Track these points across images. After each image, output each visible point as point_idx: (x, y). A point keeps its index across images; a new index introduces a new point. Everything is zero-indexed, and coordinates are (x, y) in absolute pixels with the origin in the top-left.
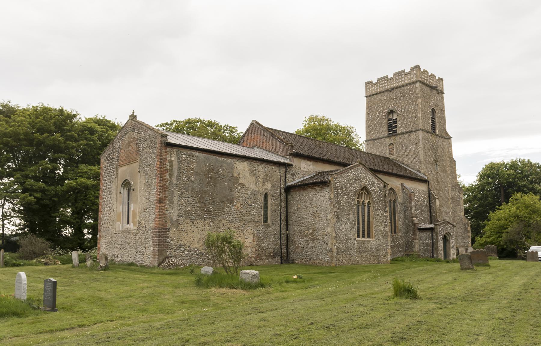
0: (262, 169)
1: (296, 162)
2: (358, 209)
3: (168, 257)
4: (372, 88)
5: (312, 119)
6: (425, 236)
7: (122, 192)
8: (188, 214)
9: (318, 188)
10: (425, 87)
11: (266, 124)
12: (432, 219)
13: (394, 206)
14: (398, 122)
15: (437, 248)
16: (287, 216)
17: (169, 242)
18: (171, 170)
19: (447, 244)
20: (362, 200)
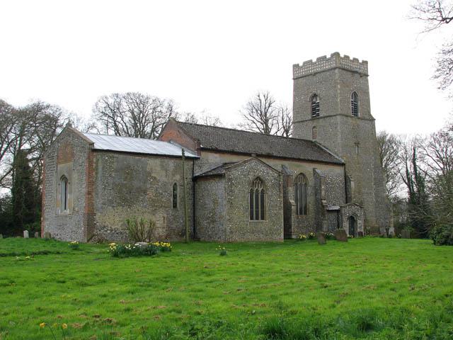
0: (171, 163)
1: (204, 154)
3: (94, 235)
6: (333, 216)
8: (111, 202)
9: (217, 180)
18: (97, 169)
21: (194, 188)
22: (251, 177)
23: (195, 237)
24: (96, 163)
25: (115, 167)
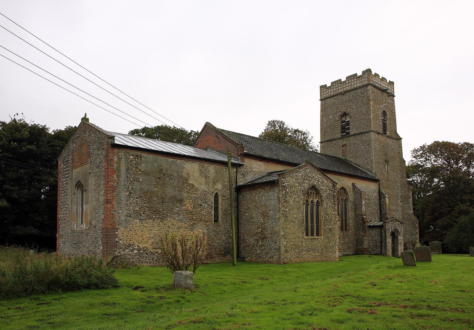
0: (212, 169)
1: (247, 162)
2: (307, 208)
4: (326, 91)
5: (272, 123)
6: (374, 233)
7: (76, 193)
9: (267, 188)
10: (376, 90)
11: (219, 125)
12: (382, 216)
13: (345, 204)
14: (351, 124)
15: (386, 245)
16: (238, 215)
17: (117, 242)
18: (119, 171)
19: (395, 241)
20: (311, 200)
21: (237, 200)
22: (306, 186)
23: (241, 259)
24: (117, 163)
25: (142, 169)
